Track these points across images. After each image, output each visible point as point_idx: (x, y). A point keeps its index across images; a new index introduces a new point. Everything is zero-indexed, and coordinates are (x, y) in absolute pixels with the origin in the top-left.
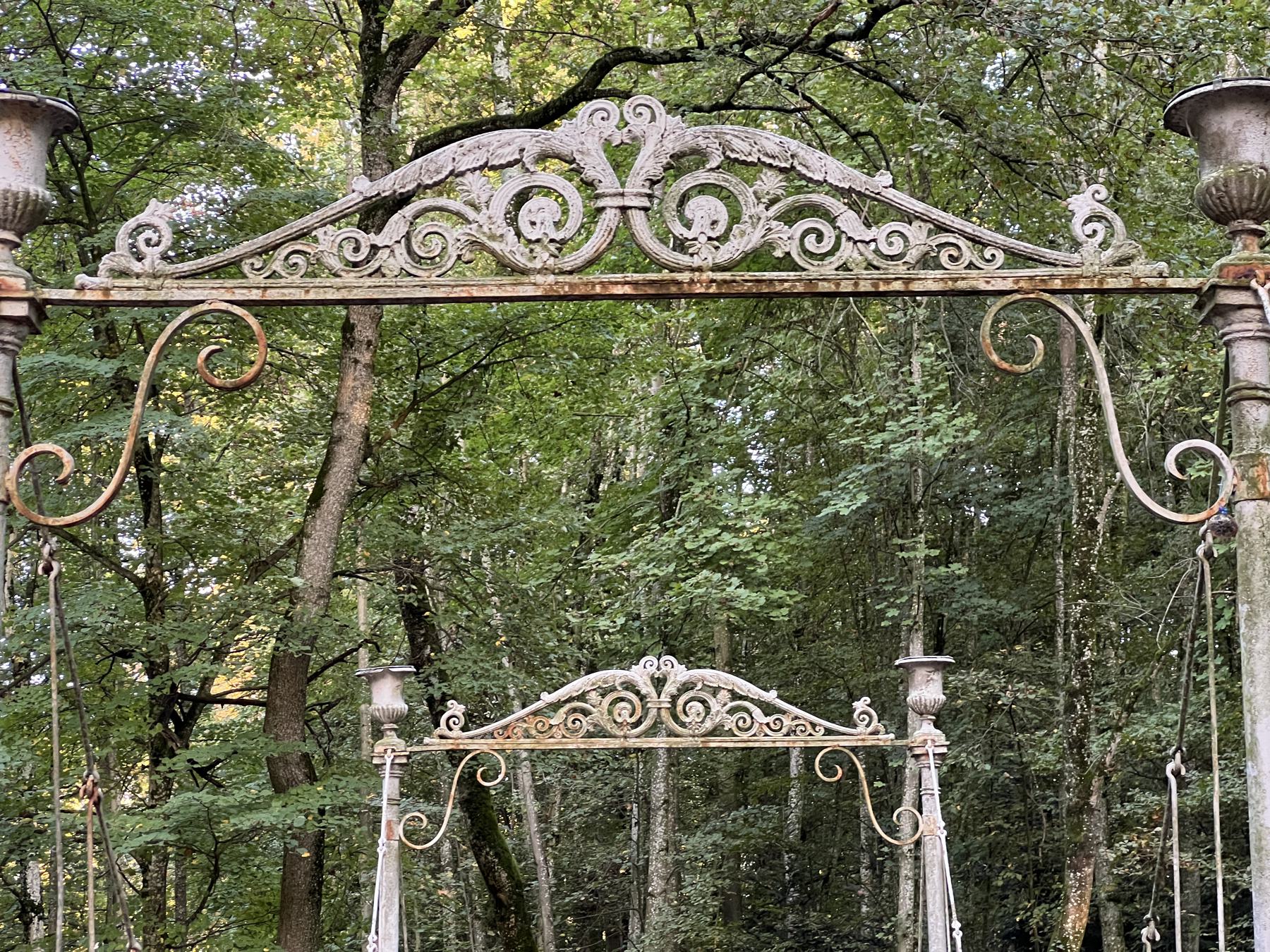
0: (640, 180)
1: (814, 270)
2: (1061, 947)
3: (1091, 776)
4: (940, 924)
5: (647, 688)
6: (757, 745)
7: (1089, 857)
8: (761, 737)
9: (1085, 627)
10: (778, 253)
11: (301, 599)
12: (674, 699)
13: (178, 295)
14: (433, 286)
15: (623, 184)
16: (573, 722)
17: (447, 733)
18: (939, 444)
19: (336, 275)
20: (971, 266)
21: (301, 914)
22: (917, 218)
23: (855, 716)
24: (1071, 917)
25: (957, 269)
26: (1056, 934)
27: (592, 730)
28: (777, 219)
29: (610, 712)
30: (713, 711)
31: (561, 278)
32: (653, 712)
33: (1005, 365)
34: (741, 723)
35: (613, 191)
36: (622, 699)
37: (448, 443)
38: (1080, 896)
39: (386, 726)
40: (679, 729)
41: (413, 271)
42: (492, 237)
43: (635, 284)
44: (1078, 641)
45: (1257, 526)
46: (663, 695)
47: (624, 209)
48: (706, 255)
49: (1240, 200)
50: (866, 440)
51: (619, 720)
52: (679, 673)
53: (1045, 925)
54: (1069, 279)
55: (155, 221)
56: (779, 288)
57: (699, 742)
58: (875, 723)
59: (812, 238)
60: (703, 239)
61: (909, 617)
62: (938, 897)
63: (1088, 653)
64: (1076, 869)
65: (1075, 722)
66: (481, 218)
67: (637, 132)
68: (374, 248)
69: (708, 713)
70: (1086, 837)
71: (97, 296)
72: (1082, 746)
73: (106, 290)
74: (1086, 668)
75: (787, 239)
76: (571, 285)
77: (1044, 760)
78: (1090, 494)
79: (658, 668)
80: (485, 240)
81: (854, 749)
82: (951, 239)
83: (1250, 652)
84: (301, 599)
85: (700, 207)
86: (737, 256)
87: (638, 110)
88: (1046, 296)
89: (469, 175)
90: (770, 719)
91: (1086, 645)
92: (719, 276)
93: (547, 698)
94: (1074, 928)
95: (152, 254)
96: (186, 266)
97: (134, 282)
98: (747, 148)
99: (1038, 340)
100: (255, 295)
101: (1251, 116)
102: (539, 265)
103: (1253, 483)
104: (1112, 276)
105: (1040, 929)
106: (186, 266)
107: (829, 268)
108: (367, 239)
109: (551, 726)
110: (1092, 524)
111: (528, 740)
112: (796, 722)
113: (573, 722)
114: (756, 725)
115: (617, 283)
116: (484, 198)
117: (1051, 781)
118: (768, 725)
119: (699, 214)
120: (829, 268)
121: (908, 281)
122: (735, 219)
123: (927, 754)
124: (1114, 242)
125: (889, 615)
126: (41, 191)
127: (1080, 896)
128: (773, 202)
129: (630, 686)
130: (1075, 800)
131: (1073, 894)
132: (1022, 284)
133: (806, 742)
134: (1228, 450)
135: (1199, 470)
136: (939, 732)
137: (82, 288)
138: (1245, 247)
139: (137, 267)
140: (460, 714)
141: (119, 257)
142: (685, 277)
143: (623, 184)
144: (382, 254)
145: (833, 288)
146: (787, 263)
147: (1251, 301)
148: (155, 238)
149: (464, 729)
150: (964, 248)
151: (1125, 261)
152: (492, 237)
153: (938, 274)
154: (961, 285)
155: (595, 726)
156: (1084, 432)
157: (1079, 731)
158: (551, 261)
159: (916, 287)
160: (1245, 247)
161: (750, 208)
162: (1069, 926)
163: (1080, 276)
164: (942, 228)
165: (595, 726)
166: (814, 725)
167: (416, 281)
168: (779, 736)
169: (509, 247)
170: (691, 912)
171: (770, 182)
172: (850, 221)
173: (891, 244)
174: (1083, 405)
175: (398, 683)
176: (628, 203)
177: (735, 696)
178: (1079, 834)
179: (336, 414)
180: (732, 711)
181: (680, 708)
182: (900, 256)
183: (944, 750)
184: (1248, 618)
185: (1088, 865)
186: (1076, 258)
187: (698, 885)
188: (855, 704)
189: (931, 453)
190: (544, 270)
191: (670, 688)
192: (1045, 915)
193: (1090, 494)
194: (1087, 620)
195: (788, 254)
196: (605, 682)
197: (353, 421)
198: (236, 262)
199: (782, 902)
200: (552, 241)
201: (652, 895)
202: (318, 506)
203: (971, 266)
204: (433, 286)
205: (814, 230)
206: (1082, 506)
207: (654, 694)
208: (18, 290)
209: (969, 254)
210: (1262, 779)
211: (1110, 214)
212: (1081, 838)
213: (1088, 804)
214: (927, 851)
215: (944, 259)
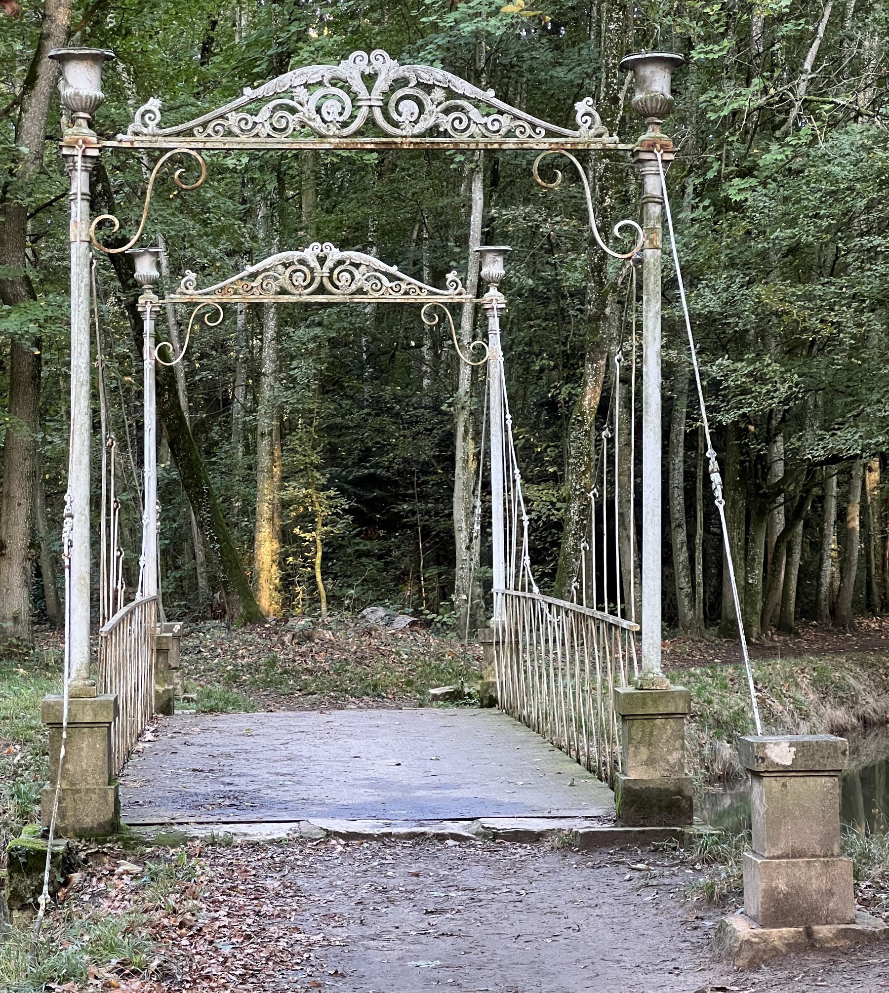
0: (378, 92)
1: (458, 138)
2: (580, 418)
3: (607, 293)
4: (498, 414)
5: (314, 264)
6: (384, 301)
7: (602, 353)
8: (387, 296)
9: (607, 180)
10: (442, 129)
11: (22, 159)
12: (332, 270)
13: (165, 145)
14: (283, 143)
15: (370, 93)
16: (267, 285)
17: (186, 291)
18: (499, 24)
19: (237, 136)
20: (530, 136)
21: (25, 393)
23: (447, 283)
24: (589, 396)
25: (523, 138)
26: (576, 409)
28: (442, 112)
30: (357, 278)
31: (342, 140)
32: (318, 280)
33: (544, 184)
34: (374, 286)
35: (365, 98)
37: (124, 32)
38: (595, 381)
39: (145, 286)
40: (335, 290)
42: (310, 119)
43: (376, 143)
44: (601, 191)
45: (652, 260)
46: (324, 268)
47: (370, 107)
48: (408, 130)
49: (652, 109)
50: (441, 17)
51: (296, 284)
52: (335, 254)
53: (570, 399)
54: (573, 144)
55: (153, 108)
56: (442, 146)
57: (347, 299)
58: (460, 287)
59: (457, 121)
60: (407, 122)
61: (471, 162)
62: (498, 398)
63: (608, 200)
64: (593, 361)
65: (596, 252)
66: (304, 109)
67: (377, 68)
69: (353, 280)
70: (602, 338)
71: (128, 145)
72: (601, 271)
73: (132, 142)
74: (606, 211)
75: (445, 122)
76: (347, 143)
77: (573, 278)
78: (615, 76)
79: (322, 251)
80: (306, 120)
81: (445, 304)
82: (521, 123)
83: (647, 317)
84: (22, 159)
85: (405, 105)
86: (423, 130)
88: (564, 152)
90: (393, 284)
91: (607, 194)
92: (414, 140)
93: (250, 269)
94: (590, 404)
95: (152, 124)
96: (168, 131)
97: (144, 138)
98: (427, 77)
99: (559, 173)
100: (200, 145)
101: (658, 69)
102: (331, 134)
103: (651, 241)
104: (595, 143)
105: (566, 402)
106: (168, 131)
107: (465, 137)
108: (251, 119)
109: (252, 288)
110: (615, 100)
112: (410, 286)
113: (267, 285)
114: (384, 288)
115: (367, 143)
116: (305, 100)
117: (579, 293)
118: (391, 288)
119: (405, 109)
120: (465, 137)
121: (501, 144)
122: (421, 112)
123: (493, 308)
124: (596, 126)
125: (457, 160)
126: (100, 94)
127: (595, 381)
128: (439, 104)
129: (302, 262)
130: (595, 310)
131: (590, 380)
132: (553, 146)
133: (416, 299)
134: (641, 224)
135: (700, 53)
136: (501, 294)
137: (121, 141)
138: (653, 130)
139: (145, 131)
140: (193, 279)
141: (136, 125)
142: (399, 140)
143: (370, 93)
144: (259, 126)
145: (467, 147)
146: (445, 134)
147: (654, 158)
148: (153, 117)
149: (196, 289)
150: (527, 128)
151: (600, 135)
152: (310, 119)
153: (514, 140)
154: (525, 146)
155: (281, 287)
156: (612, 27)
157: (599, 259)
158: (337, 132)
159: (504, 147)
160: (653, 130)
161: (429, 107)
162: (586, 403)
163: (579, 143)
164: (516, 118)
165: (281, 287)
166: (421, 289)
167: (274, 140)
168: (398, 295)
169: (317, 124)
170: (298, 388)
171: (438, 94)
172: (474, 113)
173: (493, 125)
174: (613, 5)
175: (153, 258)
176: (373, 104)
177: (451, 94)
178: (596, 335)
179: (44, 16)
181: (335, 277)
182: (498, 131)
183: (504, 306)
184: (647, 302)
185: (602, 358)
186: (577, 133)
187: (303, 369)
188: (448, 275)
189: (493, 31)
190: (334, 136)
191: (329, 264)
192: (570, 393)
193: (615, 76)
194: (608, 174)
195: (446, 130)
196: (287, 259)
197: (58, 22)
198: (191, 129)
199: (359, 376)
201: (264, 375)
202: (33, 88)
203: (530, 136)
204: (283, 143)
206: (608, 86)
207: (319, 267)
208: (93, 144)
209: (529, 131)
210: (649, 373)
211: (594, 113)
212: (597, 339)
213: (604, 314)
214: (491, 369)
215: (518, 133)
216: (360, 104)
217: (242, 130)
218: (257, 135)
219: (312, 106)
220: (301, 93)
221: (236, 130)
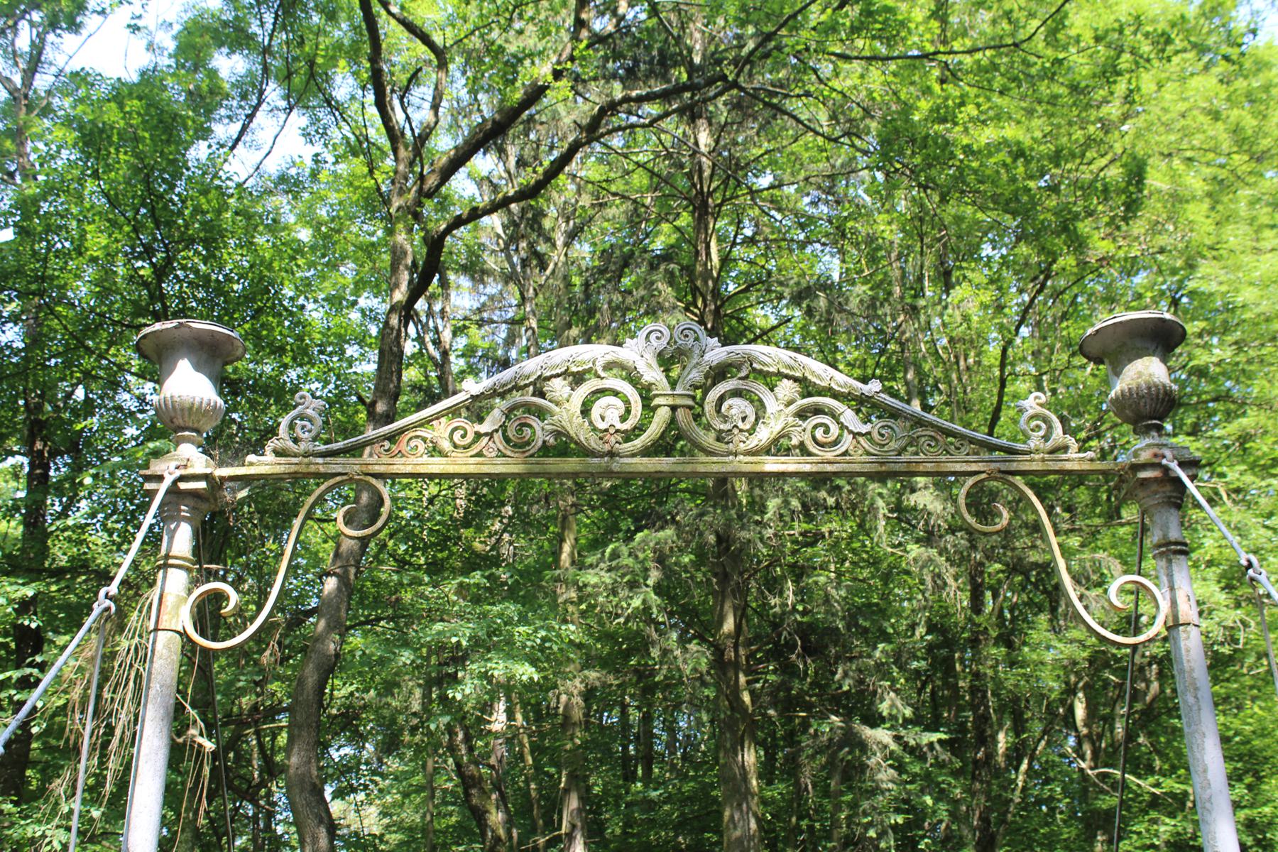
22: (942, 263)
27: (552, 441)
29: (585, 412)
34: (819, 434)
36: (602, 392)
41: (509, 453)
68: (478, 435)
87: (686, 332)
89: (553, 380)
109: (478, 435)
111: (437, 460)
116: (565, 396)
161: (772, 405)
171: (786, 389)
177: (807, 387)
180: (802, 414)
200: (617, 431)
205: (821, 425)
216: (657, 401)
217: (455, 446)
218: (479, 454)
220: (559, 387)
221: (446, 445)
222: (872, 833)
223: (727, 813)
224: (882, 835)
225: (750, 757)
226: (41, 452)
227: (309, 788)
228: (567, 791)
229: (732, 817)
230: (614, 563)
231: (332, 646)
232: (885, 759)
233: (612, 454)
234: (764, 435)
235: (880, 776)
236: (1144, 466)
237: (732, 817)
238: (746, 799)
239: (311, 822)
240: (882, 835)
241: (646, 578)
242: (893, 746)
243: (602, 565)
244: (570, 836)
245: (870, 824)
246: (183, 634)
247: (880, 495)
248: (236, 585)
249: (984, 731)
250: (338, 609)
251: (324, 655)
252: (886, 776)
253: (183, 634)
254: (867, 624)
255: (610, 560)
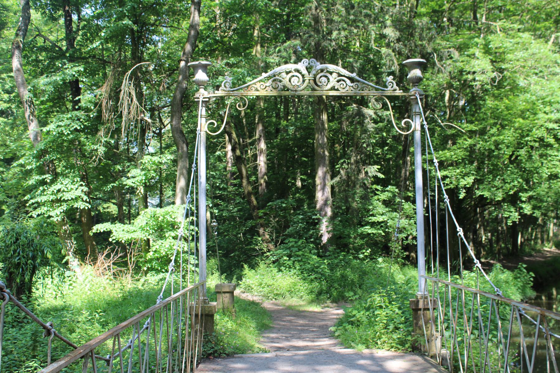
29: (290, 81)
36: (293, 76)
109: (266, 86)
118: (352, 87)
129: (298, 71)
171: (335, 75)
177: (340, 75)
180: (338, 81)
219: (287, 79)
221: (259, 89)
222: (365, 145)
223: (317, 136)
224: (368, 146)
225: (325, 117)
226: (68, 11)
227: (179, 131)
228: (258, 123)
229: (318, 137)
230: (279, 54)
231: (185, 85)
232: (371, 120)
233: (296, 91)
234: (329, 86)
235: (369, 126)
236: (412, 96)
237: (318, 137)
238: (323, 131)
239: (181, 143)
240: (368, 146)
241: (290, 60)
242: (374, 116)
243: (275, 54)
244: (259, 139)
245: (364, 143)
246: (206, 132)
247: (373, 30)
248: (217, 122)
249: (408, 108)
250: (186, 72)
251: (182, 88)
252: (371, 126)
253: (206, 132)
254: (366, 76)
255: (278, 53)
